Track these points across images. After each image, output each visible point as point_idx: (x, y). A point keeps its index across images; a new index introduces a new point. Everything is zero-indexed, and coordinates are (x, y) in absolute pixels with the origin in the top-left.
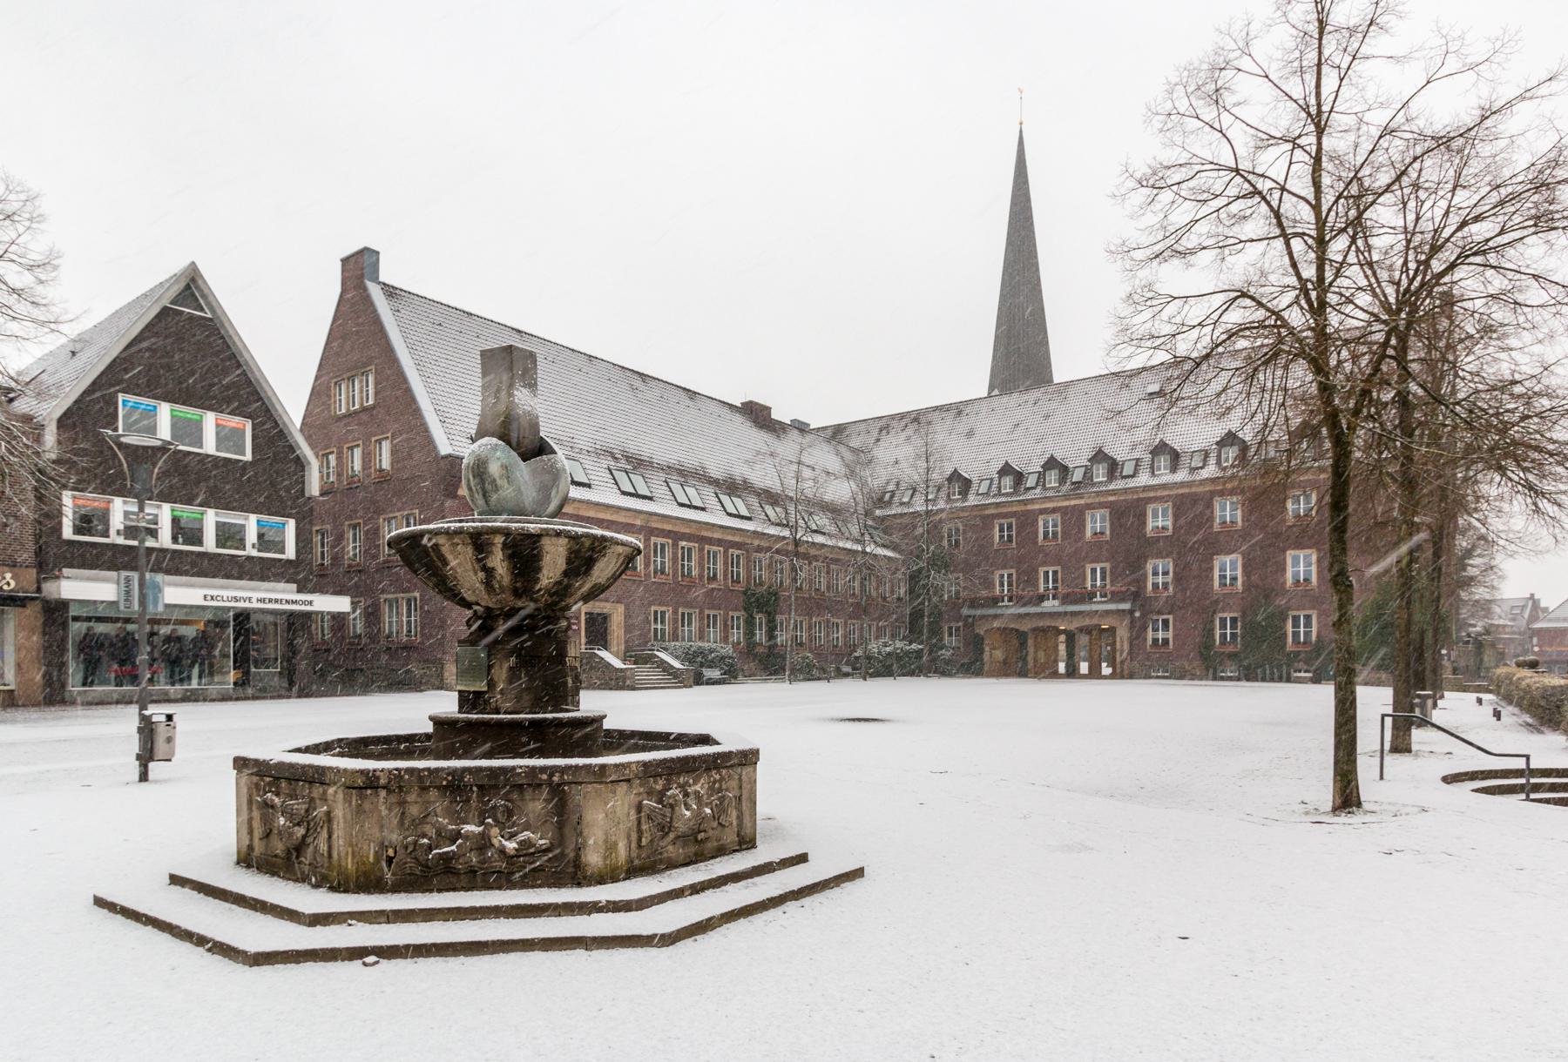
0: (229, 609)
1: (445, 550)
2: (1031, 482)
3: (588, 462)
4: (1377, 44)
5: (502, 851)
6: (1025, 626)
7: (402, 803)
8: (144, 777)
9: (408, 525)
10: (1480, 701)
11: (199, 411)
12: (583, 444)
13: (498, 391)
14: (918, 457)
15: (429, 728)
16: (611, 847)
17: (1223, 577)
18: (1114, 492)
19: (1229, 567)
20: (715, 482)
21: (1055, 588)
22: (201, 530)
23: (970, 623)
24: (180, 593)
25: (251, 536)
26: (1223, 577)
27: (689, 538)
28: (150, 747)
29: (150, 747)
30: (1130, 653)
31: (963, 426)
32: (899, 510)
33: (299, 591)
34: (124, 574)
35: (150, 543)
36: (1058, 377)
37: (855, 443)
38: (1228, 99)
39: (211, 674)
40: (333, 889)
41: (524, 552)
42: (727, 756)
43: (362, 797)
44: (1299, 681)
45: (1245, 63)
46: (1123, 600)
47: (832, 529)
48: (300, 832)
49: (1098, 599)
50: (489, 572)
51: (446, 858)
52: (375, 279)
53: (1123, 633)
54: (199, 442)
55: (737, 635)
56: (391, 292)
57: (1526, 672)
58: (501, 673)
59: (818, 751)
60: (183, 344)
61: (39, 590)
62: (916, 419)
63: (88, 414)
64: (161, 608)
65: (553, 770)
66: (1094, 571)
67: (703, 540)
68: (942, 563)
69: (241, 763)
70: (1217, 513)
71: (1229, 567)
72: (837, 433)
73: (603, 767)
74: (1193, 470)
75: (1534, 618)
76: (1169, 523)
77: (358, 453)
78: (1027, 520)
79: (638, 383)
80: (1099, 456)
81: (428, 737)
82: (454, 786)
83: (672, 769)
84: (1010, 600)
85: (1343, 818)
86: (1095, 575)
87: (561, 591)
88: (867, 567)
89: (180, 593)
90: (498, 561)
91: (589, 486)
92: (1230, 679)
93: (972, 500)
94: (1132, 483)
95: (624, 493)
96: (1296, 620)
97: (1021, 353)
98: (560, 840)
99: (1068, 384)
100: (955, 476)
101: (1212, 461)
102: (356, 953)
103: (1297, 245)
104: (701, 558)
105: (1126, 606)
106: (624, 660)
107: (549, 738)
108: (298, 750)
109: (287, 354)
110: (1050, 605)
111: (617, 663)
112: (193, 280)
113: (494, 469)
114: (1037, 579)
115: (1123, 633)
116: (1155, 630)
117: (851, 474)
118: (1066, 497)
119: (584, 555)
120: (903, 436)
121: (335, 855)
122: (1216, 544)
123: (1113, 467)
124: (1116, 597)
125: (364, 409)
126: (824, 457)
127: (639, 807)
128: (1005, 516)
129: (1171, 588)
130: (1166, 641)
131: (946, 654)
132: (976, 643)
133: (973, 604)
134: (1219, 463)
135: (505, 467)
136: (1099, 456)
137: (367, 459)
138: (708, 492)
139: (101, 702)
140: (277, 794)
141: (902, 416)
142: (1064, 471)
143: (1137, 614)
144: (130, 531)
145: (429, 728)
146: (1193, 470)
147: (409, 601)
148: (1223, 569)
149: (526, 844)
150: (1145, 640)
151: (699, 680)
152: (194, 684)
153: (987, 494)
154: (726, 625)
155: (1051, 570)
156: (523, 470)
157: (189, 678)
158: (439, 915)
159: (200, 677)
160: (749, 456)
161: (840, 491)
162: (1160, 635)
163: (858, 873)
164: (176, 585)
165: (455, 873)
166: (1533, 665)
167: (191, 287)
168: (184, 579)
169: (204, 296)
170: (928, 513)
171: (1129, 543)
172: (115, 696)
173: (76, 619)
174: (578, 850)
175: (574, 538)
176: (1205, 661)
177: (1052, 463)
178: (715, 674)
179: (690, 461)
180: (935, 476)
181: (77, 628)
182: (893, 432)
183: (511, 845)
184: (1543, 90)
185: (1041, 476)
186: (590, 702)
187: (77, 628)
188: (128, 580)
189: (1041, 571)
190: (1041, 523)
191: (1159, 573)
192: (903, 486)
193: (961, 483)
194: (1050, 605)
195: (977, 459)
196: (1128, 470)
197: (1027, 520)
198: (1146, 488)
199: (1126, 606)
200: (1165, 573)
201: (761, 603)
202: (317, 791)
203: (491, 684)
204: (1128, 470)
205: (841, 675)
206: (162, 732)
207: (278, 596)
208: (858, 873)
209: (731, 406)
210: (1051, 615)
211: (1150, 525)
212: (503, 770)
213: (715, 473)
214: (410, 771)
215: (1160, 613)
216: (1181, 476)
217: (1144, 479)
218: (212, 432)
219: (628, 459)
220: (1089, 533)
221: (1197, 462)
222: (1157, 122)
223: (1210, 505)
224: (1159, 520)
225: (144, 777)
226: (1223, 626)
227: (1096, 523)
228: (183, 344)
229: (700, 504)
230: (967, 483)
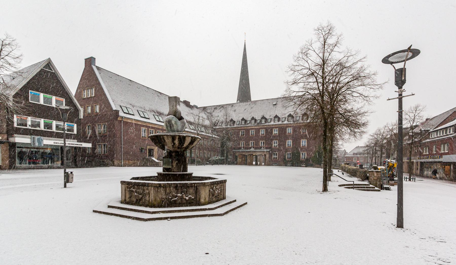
0: (59, 146)
1: (166, 139)
2: (248, 122)
3: (148, 113)
4: (336, 49)
5: (185, 199)
7: (166, 191)
8: (65, 186)
9: (156, 133)
10: (339, 171)
11: (50, 96)
12: (147, 109)
13: (173, 106)
15: (157, 175)
16: (205, 199)
17: (288, 145)
18: (266, 125)
19: (289, 142)
22: (52, 126)
24: (48, 142)
25: (29, 123)
26: (288, 145)
28: (68, 179)
29: (68, 179)
31: (234, 108)
32: (220, 127)
33: (77, 142)
34: (33, 136)
35: (38, 129)
36: (253, 99)
37: (209, 111)
38: (308, 55)
39: (54, 162)
40: (150, 207)
41: (182, 139)
42: (220, 181)
43: (158, 189)
44: (302, 166)
45: (311, 48)
46: (268, 149)
47: (204, 131)
48: (141, 196)
50: (174, 144)
51: (175, 201)
52: (95, 65)
54: (39, 101)
56: (98, 68)
57: (347, 166)
58: (174, 164)
59: (238, 179)
60: (46, 78)
61: (8, 140)
62: (222, 106)
63: (22, 94)
64: (42, 145)
65: (195, 183)
68: (229, 139)
70: (287, 131)
71: (289, 142)
72: (204, 109)
73: (205, 183)
74: (282, 121)
75: (345, 154)
76: (277, 133)
77: (90, 108)
78: (248, 131)
79: (159, 95)
80: (263, 117)
81: (157, 176)
82: (176, 186)
83: (213, 183)
85: (325, 193)
86: (261, 143)
87: (187, 148)
88: (213, 140)
89: (48, 142)
90: (177, 142)
91: (149, 119)
92: (303, 167)
94: (270, 124)
95: (141, 117)
96: (302, 154)
97: (244, 94)
98: (196, 197)
99: (255, 102)
100: (232, 120)
101: (286, 120)
102: (172, 218)
103: (320, 85)
105: (268, 150)
106: (158, 159)
107: (183, 177)
109: (72, 81)
110: (252, 149)
111: (157, 161)
112: (49, 62)
113: (173, 122)
117: (208, 119)
118: (256, 126)
119: (193, 140)
121: (150, 201)
122: (287, 138)
123: (266, 120)
124: (267, 148)
125: (91, 97)
126: (203, 115)
127: (210, 191)
130: (276, 158)
131: (229, 160)
132: (236, 157)
133: (234, 149)
134: (288, 120)
135: (175, 122)
136: (263, 117)
137: (92, 110)
139: (25, 169)
141: (219, 106)
142: (256, 120)
144: (32, 126)
145: (157, 175)
146: (282, 121)
147: (104, 145)
148: (288, 143)
149: (190, 198)
152: (50, 164)
153: (239, 125)
156: (179, 123)
157: (48, 163)
158: (176, 211)
159: (51, 163)
160: (187, 114)
161: (207, 123)
162: (275, 156)
163: (246, 203)
164: (46, 139)
165: (176, 203)
166: (348, 164)
167: (49, 64)
168: (51, 138)
169: (52, 67)
170: (226, 128)
171: (268, 138)
172: (47, 167)
173: (18, 147)
174: (199, 199)
175: (192, 137)
176: (284, 162)
177: (253, 118)
180: (228, 120)
181: (18, 150)
183: (187, 198)
184: (363, 60)
187: (18, 150)
188: (34, 138)
189: (261, 141)
191: (275, 144)
192: (220, 121)
193: (233, 121)
194: (252, 149)
196: (269, 121)
197: (248, 131)
198: (273, 125)
199: (268, 150)
200: (276, 143)
202: (145, 188)
203: (172, 166)
204: (269, 121)
205: (207, 164)
206: (71, 175)
207: (71, 143)
208: (246, 203)
210: (252, 152)
211: (273, 133)
212: (186, 183)
214: (167, 184)
216: (280, 123)
217: (272, 123)
218: (54, 101)
219: (158, 112)
221: (284, 120)
222: (296, 58)
223: (286, 129)
224: (275, 132)
225: (65, 186)
226: (288, 155)
227: (262, 132)
228: (46, 78)
230: (234, 122)
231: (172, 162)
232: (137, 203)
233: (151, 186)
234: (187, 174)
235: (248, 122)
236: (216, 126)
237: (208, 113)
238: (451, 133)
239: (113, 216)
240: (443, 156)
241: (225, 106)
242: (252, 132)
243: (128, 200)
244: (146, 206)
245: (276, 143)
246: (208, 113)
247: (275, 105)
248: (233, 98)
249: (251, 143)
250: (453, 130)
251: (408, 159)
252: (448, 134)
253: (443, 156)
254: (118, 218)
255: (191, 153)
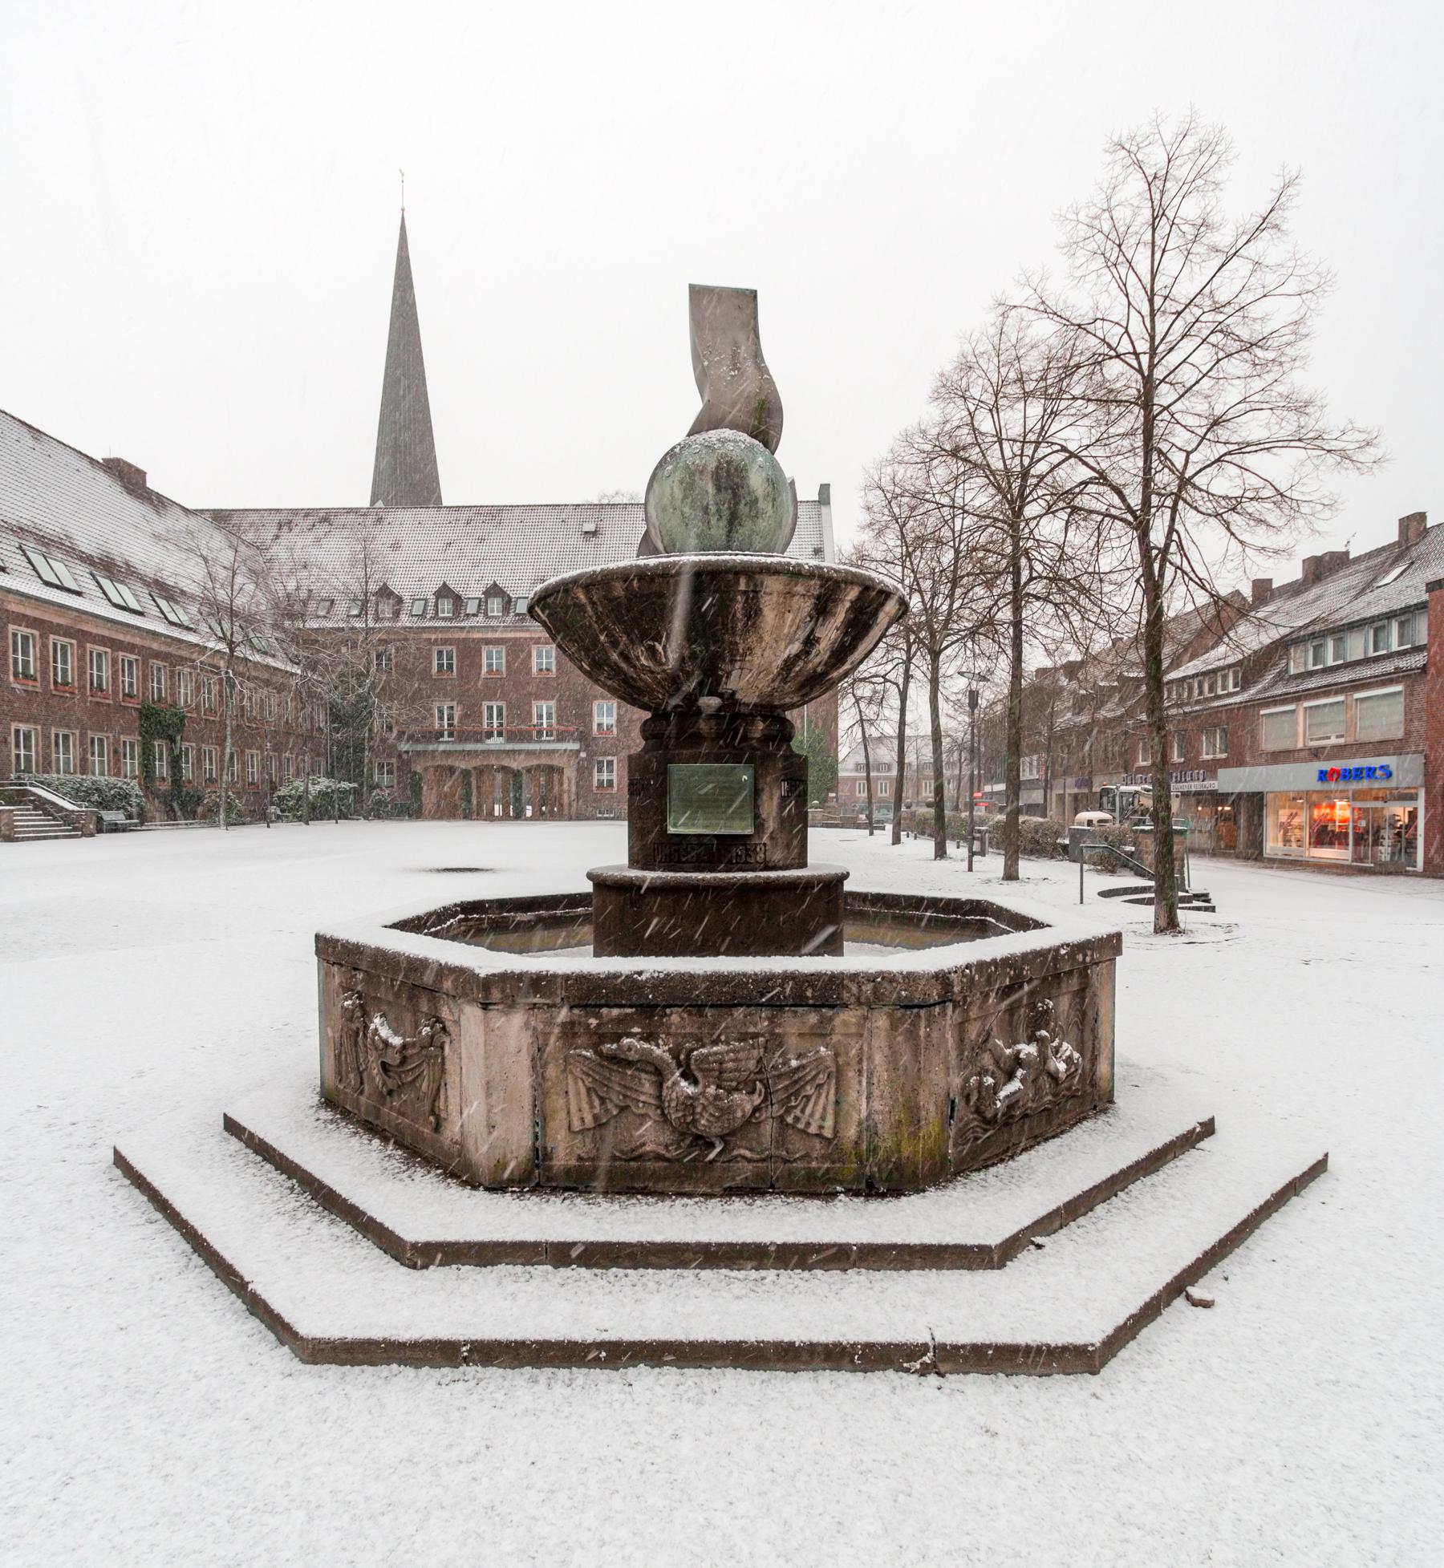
2: (472, 608)
6: (515, 764)
14: (353, 562)
15: (588, 887)
20: (87, 560)
21: (501, 725)
23: (405, 763)
27: (68, 632)
30: (577, 794)
48: (744, 1102)
49: (446, 738)
50: (810, 642)
53: (570, 773)
55: (132, 765)
66: (490, 708)
67: (83, 637)
69: (330, 950)
72: (220, 518)
78: (469, 651)
84: (451, 735)
93: (405, 621)
97: (406, 462)
100: (385, 592)
104: (81, 659)
105: (576, 746)
108: (406, 926)
110: (496, 743)
114: (481, 716)
115: (570, 773)
116: (600, 770)
120: (311, 536)
128: (445, 642)
129: (615, 729)
130: (610, 782)
138: (83, 570)
140: (649, 1037)
141: (308, 513)
143: (583, 755)
145: (588, 887)
150: (591, 781)
151: (102, 827)
153: (422, 616)
154: (116, 752)
155: (495, 705)
162: (605, 776)
177: (494, 591)
178: (118, 817)
179: (51, 526)
182: (296, 530)
185: (482, 606)
186: (830, 850)
189: (485, 704)
190: (484, 655)
194: (496, 743)
195: (331, 566)
197: (469, 651)
201: (158, 724)
202: (793, 1024)
203: (759, 826)
209: (92, 461)
213: (87, 546)
215: (605, 754)
220: (534, 670)
229: (74, 587)
231: (757, 793)
232: (691, 1165)
233: (875, 1001)
234: (808, 884)
235: (472, 608)
236: (302, 616)
237: (249, 545)
238: (1231, 689)
239: (643, 1376)
240: (1221, 772)
241: (342, 519)
242: (493, 659)
243: (564, 1153)
244: (815, 1187)
245: (610, 714)
246: (249, 545)
247: (594, 534)
248: (352, 486)
249: (492, 712)
250: (1236, 677)
251: (1078, 785)
252: (1220, 692)
253: (1221, 772)
254: (733, 1381)
255: (175, 763)
